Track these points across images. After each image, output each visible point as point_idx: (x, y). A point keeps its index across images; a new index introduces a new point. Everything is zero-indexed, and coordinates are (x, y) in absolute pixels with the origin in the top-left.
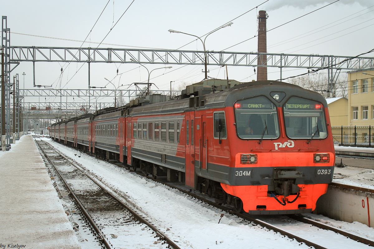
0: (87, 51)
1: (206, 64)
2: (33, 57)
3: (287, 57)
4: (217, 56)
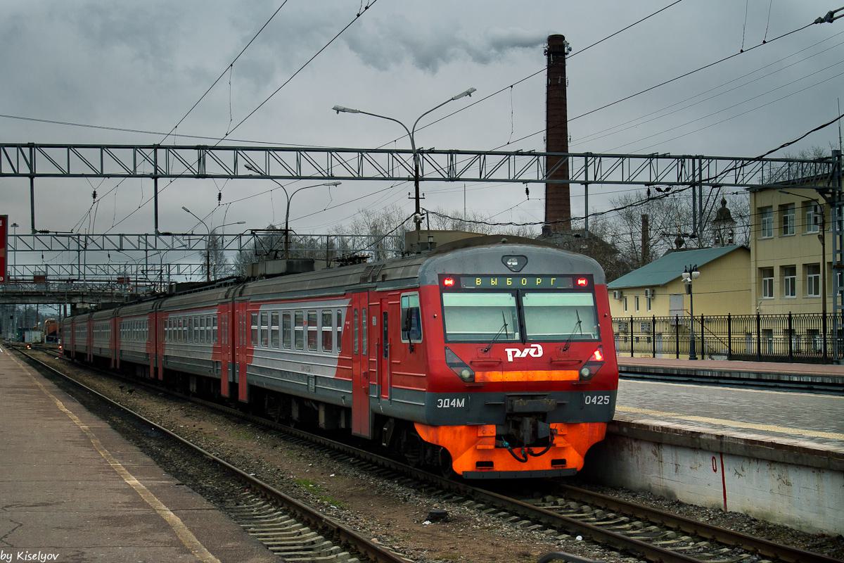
0: (150, 152)
1: (417, 179)
2: (30, 166)
3: (600, 160)
4: (443, 160)
